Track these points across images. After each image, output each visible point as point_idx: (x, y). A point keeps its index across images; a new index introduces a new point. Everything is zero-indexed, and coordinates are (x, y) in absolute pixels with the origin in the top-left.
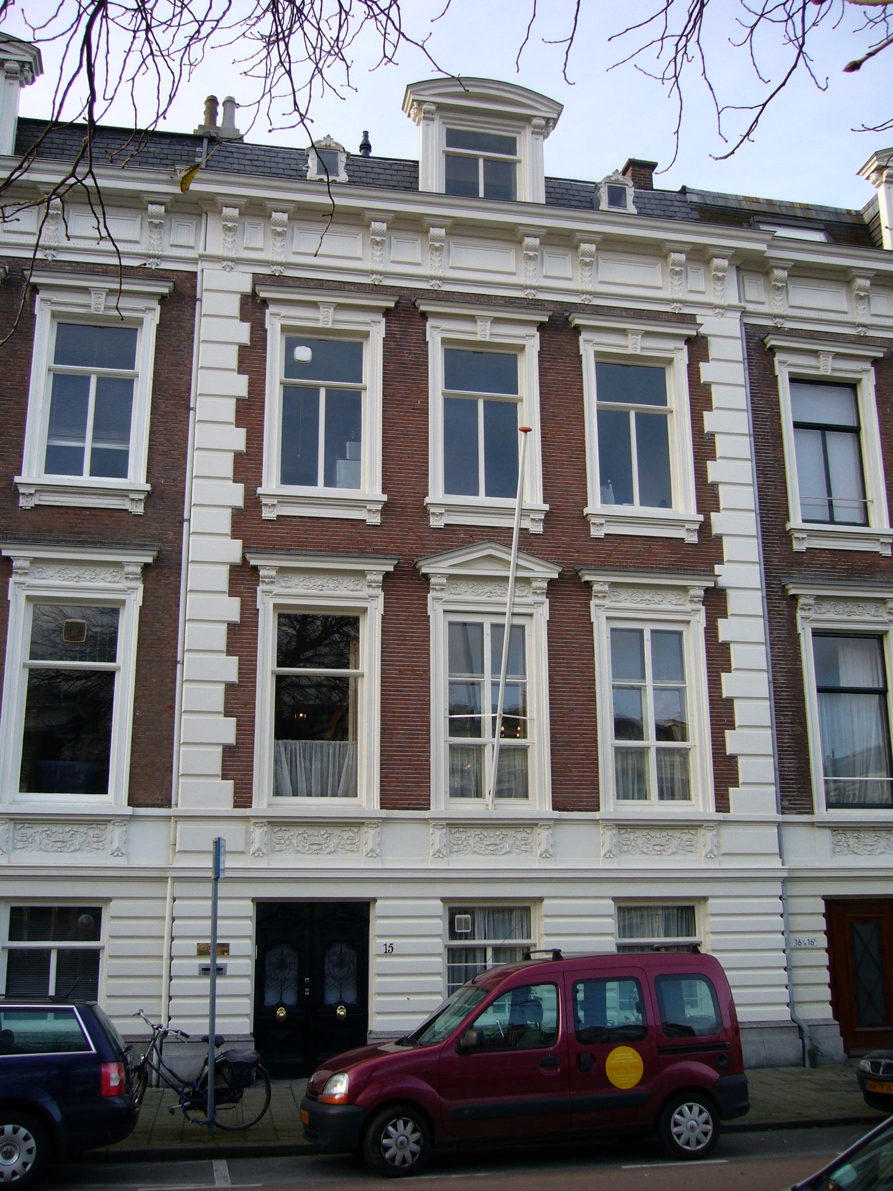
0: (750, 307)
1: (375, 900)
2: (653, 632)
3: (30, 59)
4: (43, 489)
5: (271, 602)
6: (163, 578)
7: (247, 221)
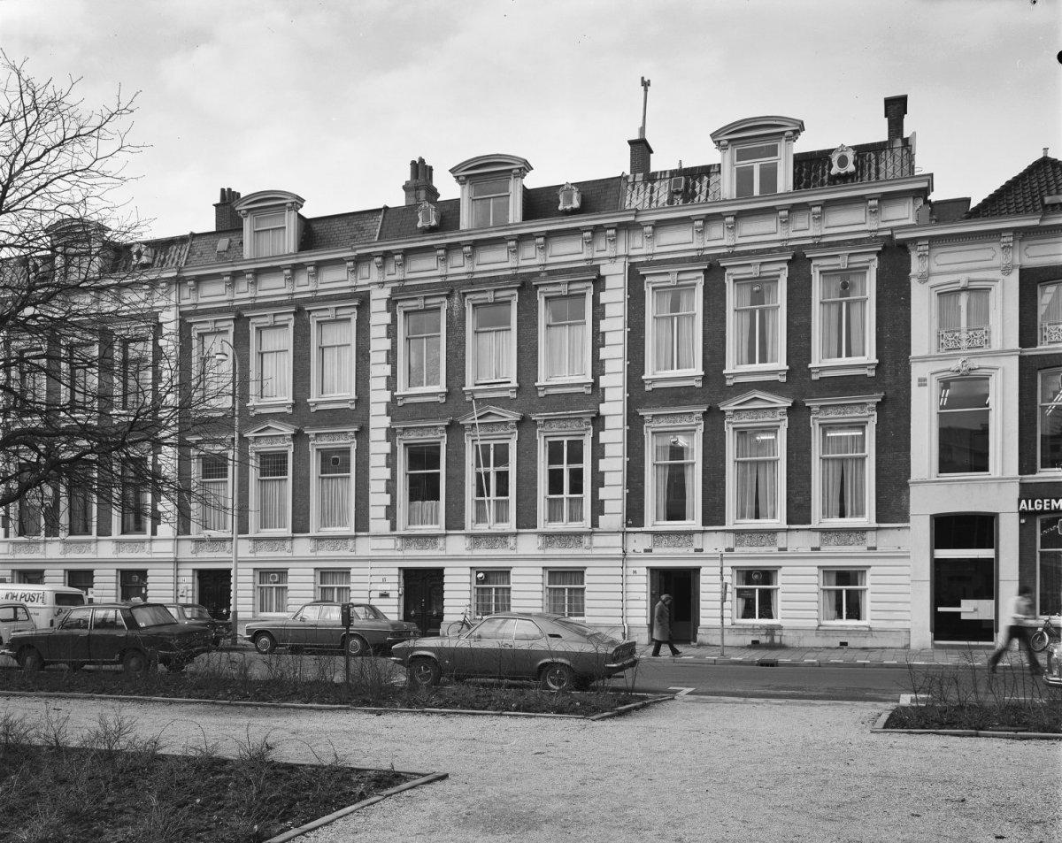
0: (632, 253)
2: (568, 441)
6: (362, 433)
7: (521, 244)
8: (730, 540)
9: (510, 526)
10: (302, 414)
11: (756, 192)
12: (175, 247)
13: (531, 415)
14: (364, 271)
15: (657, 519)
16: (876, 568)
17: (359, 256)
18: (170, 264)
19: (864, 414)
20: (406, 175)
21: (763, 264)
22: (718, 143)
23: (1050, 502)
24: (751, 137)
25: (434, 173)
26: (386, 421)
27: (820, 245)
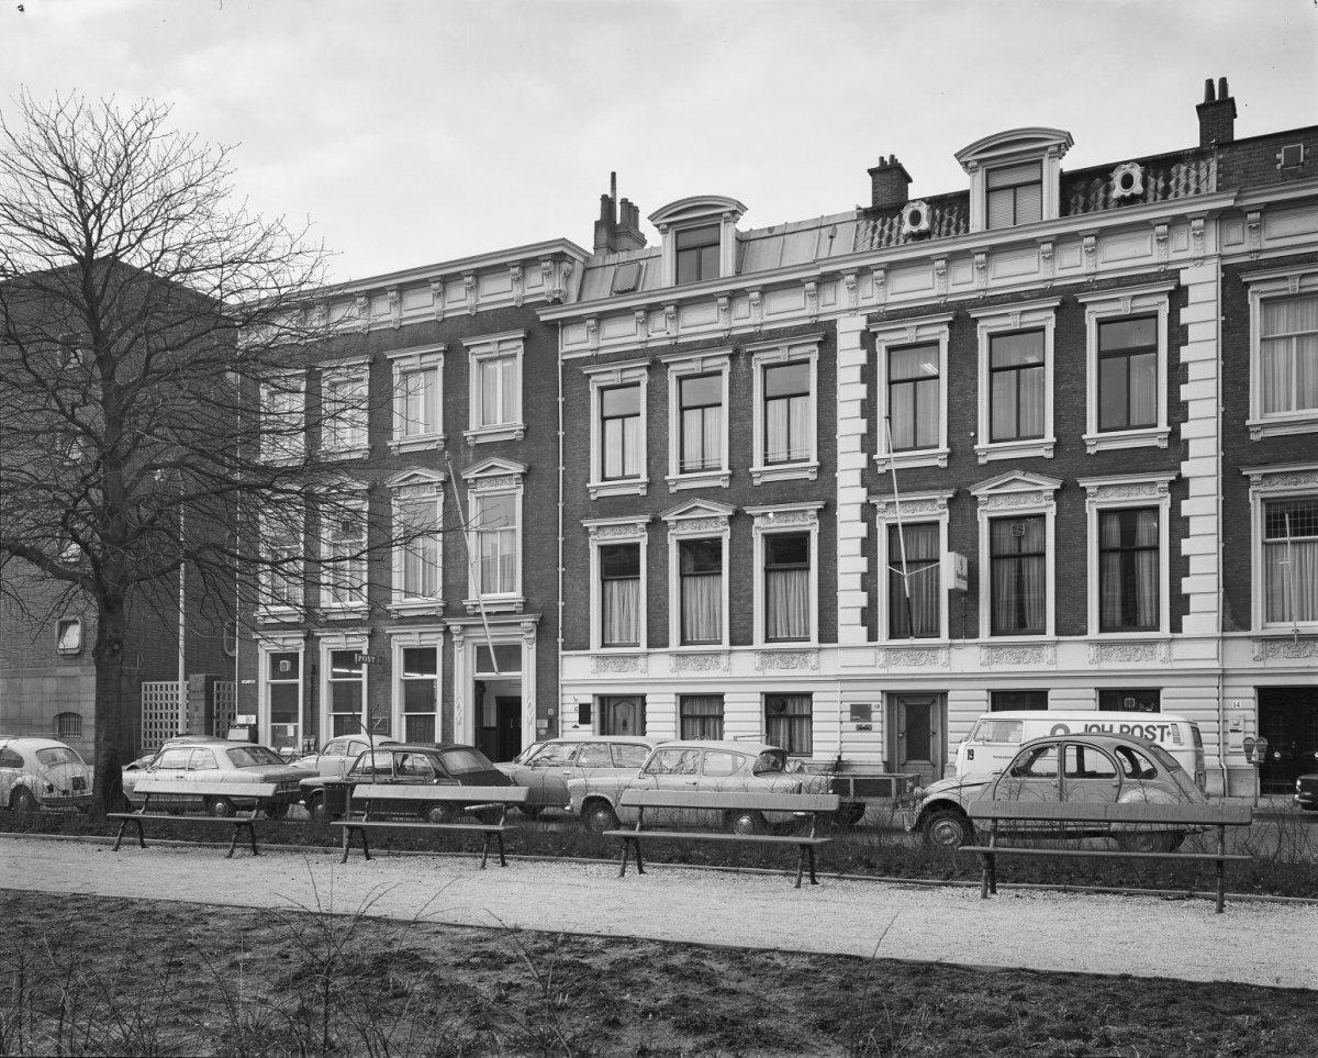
1: (1162, 688)
3: (1065, 141)
4: (1099, 441)
5: (596, 544)
6: (827, 514)
7: (952, 265)
10: (741, 493)
12: (1183, 168)
13: (745, 508)
14: (828, 295)
16: (1169, 689)
17: (823, 276)
18: (1182, 195)
19: (1153, 496)
20: (596, 214)
21: (1135, 297)
22: (965, 165)
25: (1236, 102)
26: (861, 495)
27: (677, 348)
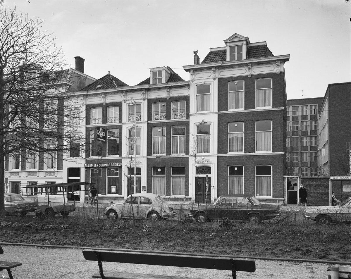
8: (26, 174)
9: (37, 170)
11: (236, 59)
15: (13, 168)
23: (91, 165)
24: (234, 40)
25: (85, 63)
